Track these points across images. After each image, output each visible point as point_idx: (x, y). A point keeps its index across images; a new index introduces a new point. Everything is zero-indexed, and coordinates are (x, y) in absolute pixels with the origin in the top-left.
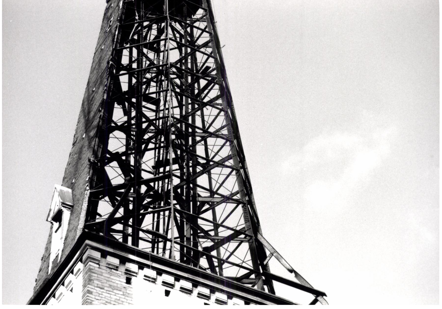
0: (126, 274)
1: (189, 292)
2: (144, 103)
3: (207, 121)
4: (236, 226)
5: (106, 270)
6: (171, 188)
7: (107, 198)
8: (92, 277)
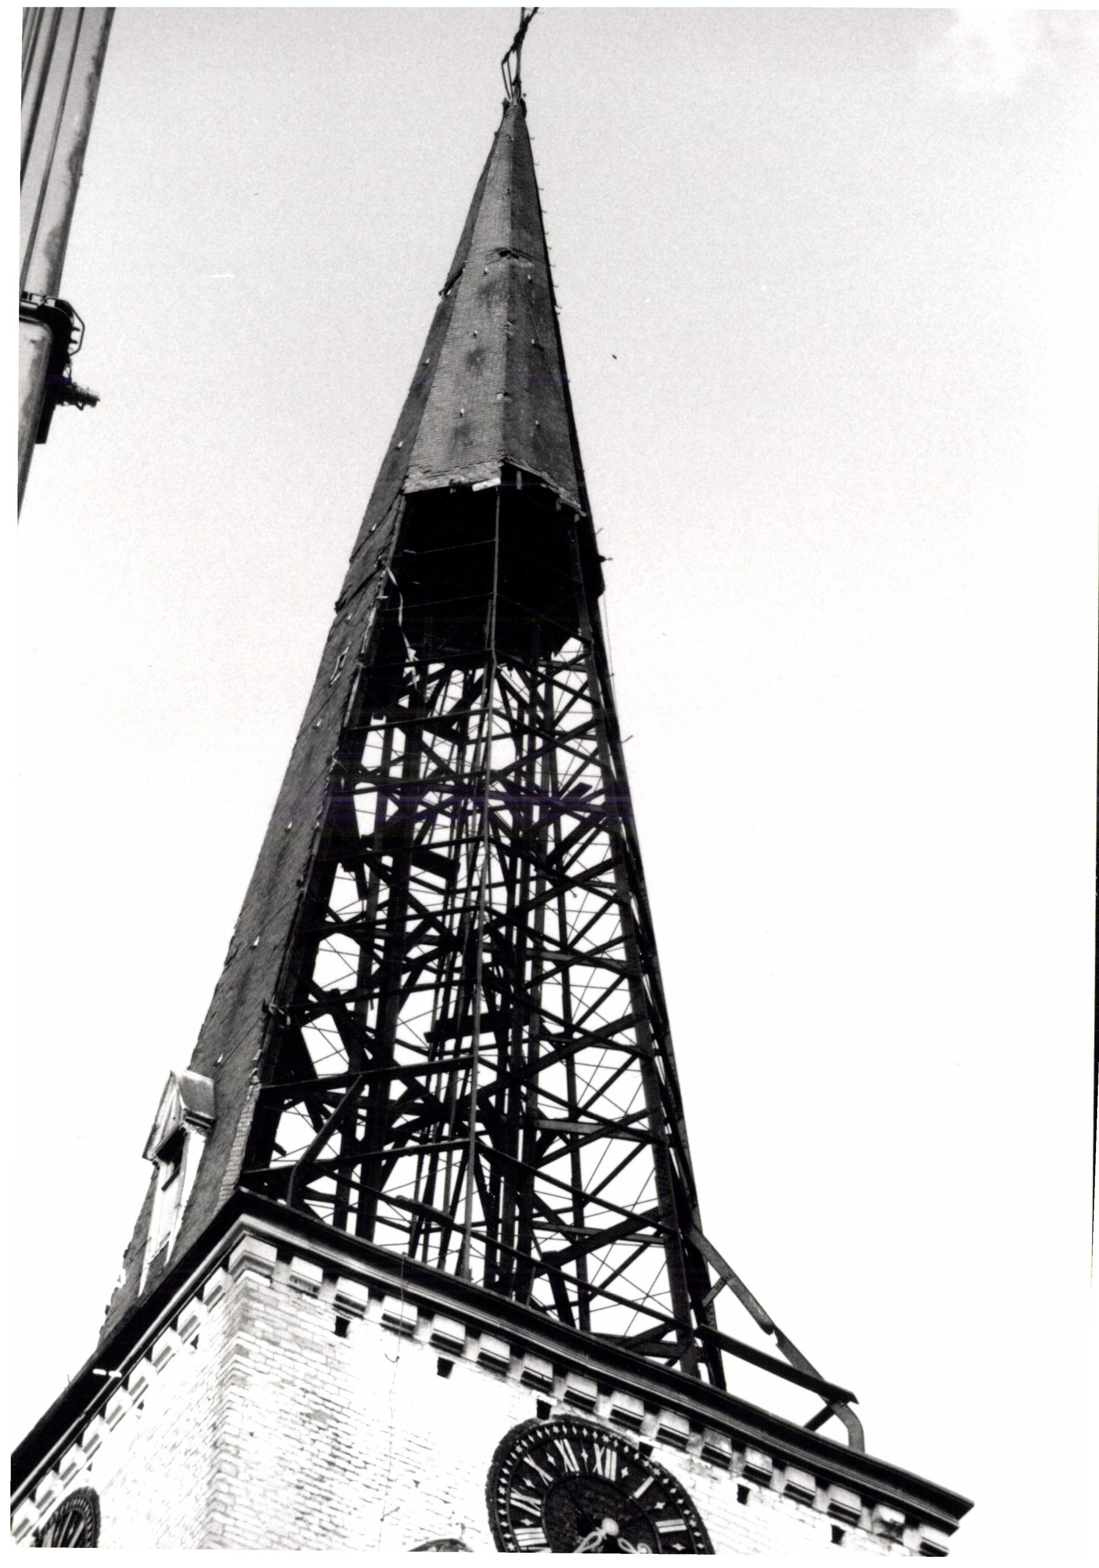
0: (337, 1307)
2: (414, 871)
3: (572, 924)
4: (634, 1202)
5: (289, 1296)
6: (471, 1093)
7: (302, 1107)
8: (251, 1311)
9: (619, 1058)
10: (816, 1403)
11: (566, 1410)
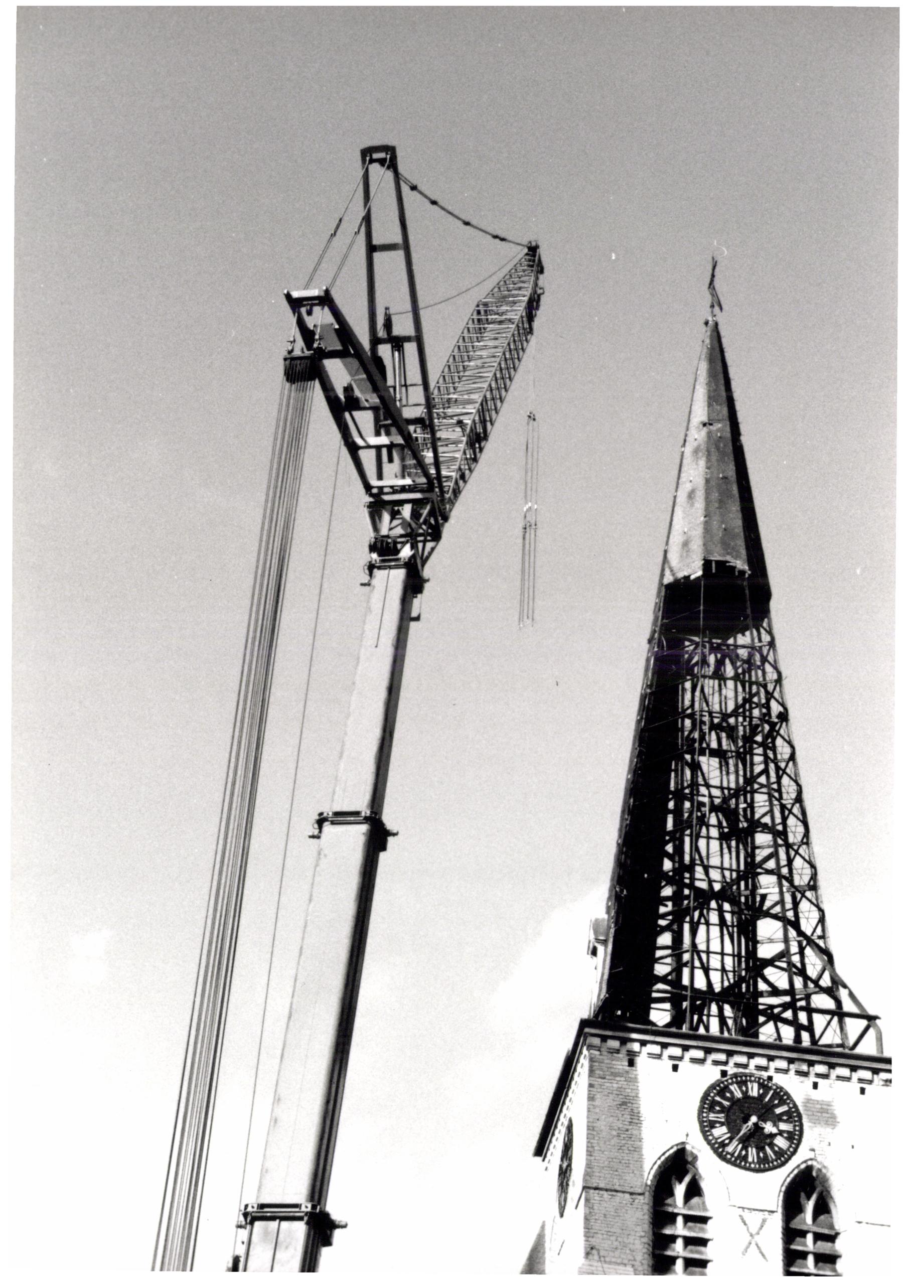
0: (628, 1055)
1: (702, 1061)
11: (736, 1070)
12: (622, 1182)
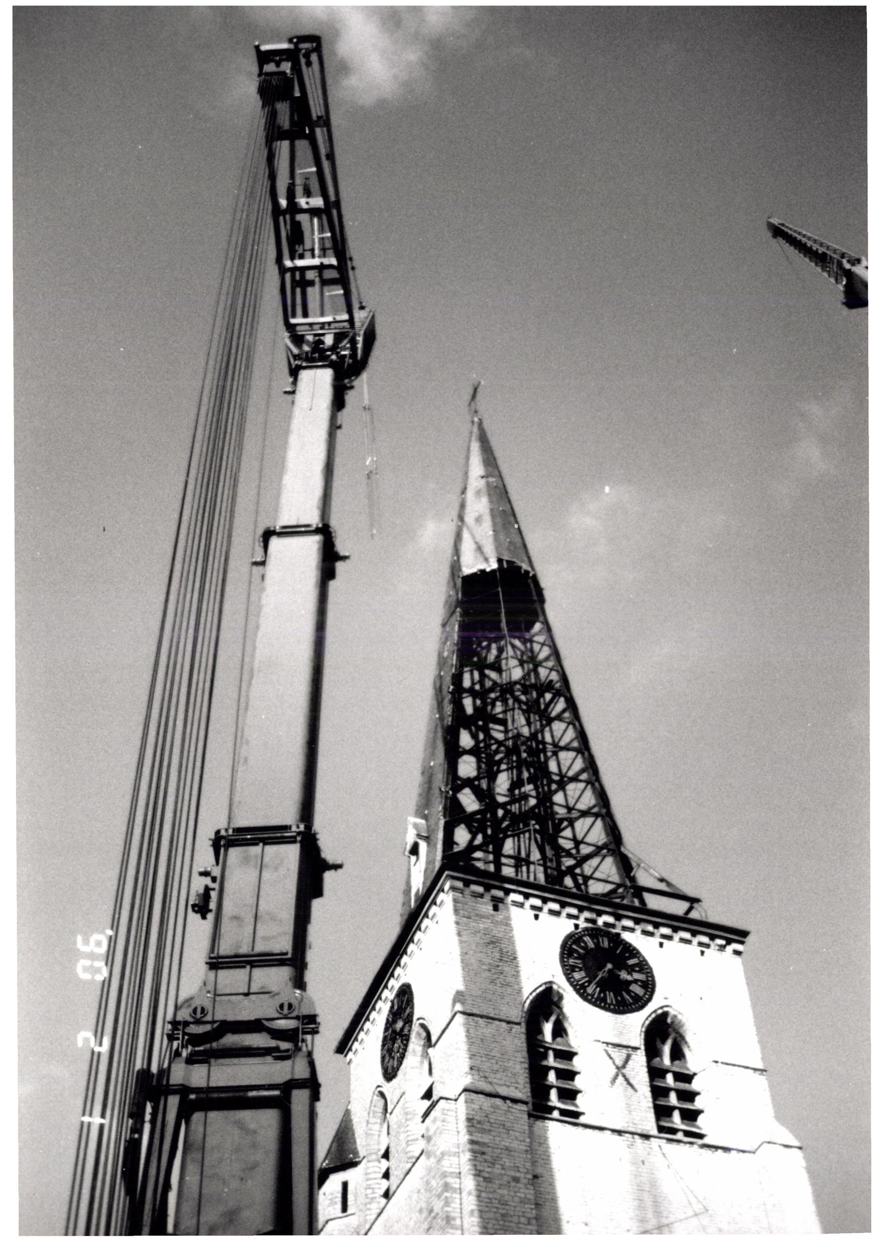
0: (492, 900)
2: (491, 725)
7: (463, 826)
9: (582, 785)
10: (685, 905)
12: (497, 1012)
